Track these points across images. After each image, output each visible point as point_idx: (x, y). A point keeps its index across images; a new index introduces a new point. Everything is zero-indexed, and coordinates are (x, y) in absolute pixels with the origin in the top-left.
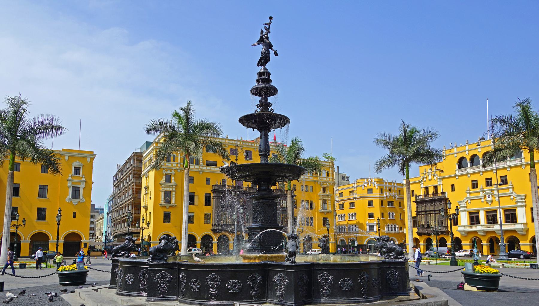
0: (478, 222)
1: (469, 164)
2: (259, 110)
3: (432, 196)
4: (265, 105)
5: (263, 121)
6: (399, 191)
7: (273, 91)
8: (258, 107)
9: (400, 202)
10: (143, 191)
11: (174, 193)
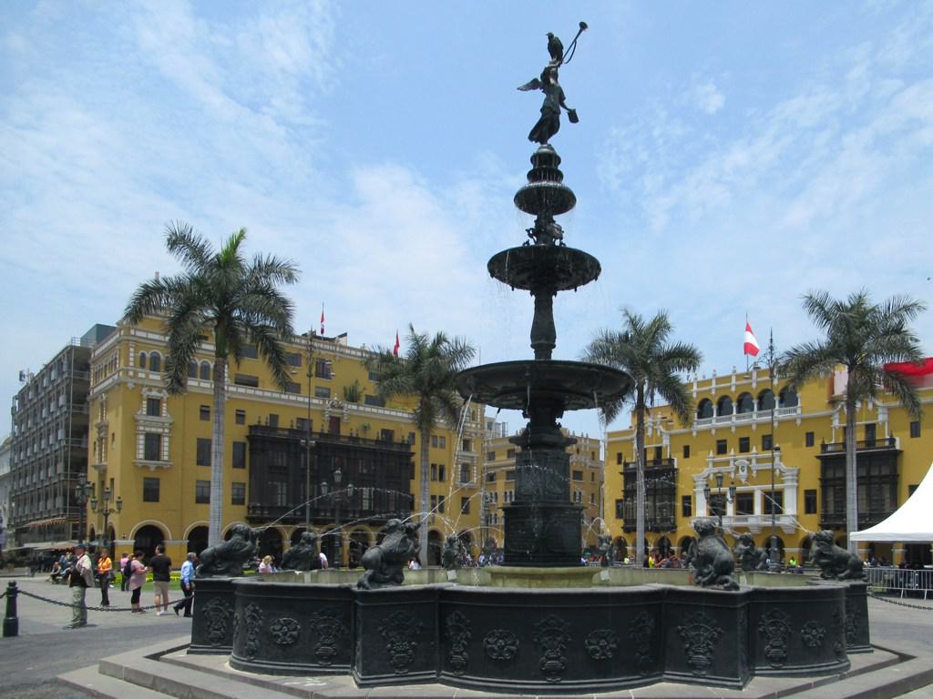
0: (750, 510)
1: (734, 409)
3: (651, 464)
4: (544, 230)
5: (544, 268)
6: (593, 453)
7: (565, 201)
8: (531, 236)
9: (593, 474)
10: (93, 434)
11: (166, 439)
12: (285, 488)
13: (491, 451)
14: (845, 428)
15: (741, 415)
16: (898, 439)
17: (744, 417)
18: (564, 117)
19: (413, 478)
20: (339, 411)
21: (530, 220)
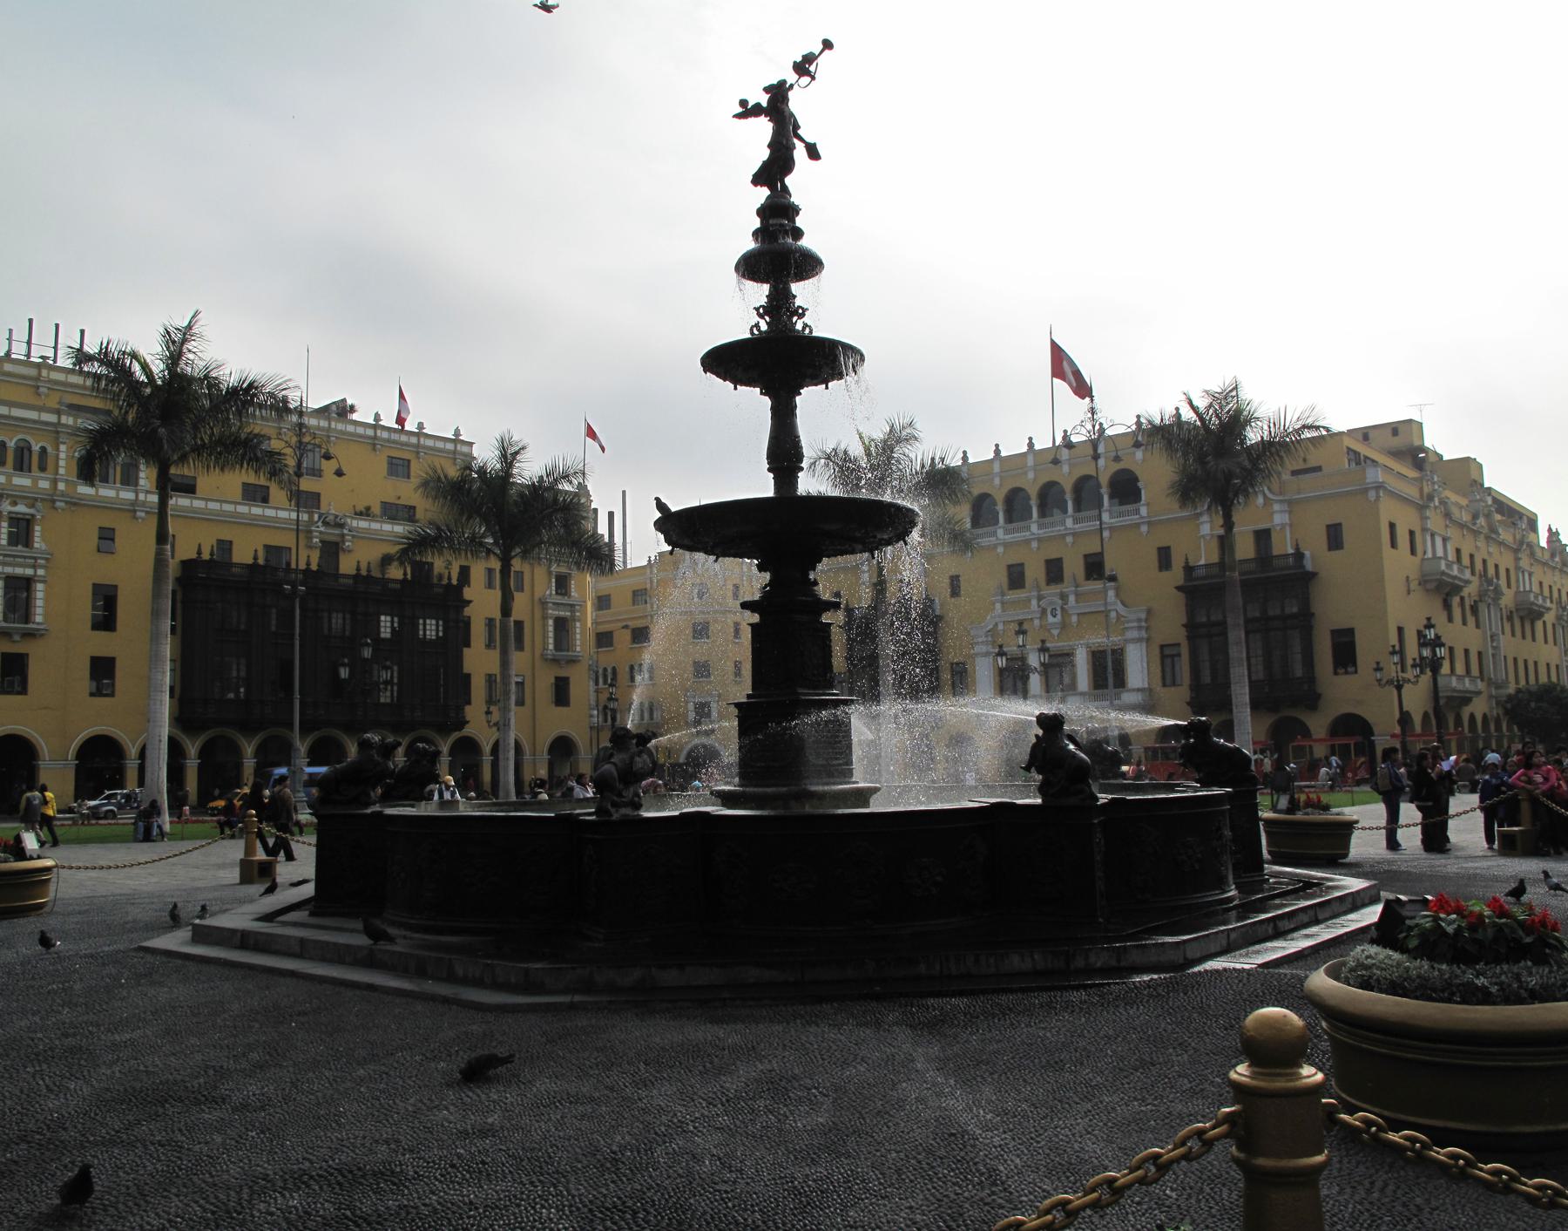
2: (764, 327)
4: (780, 307)
7: (808, 265)
8: (761, 316)
12: (243, 668)
13: (700, 618)
14: (1221, 538)
15: (1047, 520)
16: (1307, 553)
17: (1052, 525)
18: (800, 153)
19: (468, 645)
20: (337, 532)
21: (759, 293)
